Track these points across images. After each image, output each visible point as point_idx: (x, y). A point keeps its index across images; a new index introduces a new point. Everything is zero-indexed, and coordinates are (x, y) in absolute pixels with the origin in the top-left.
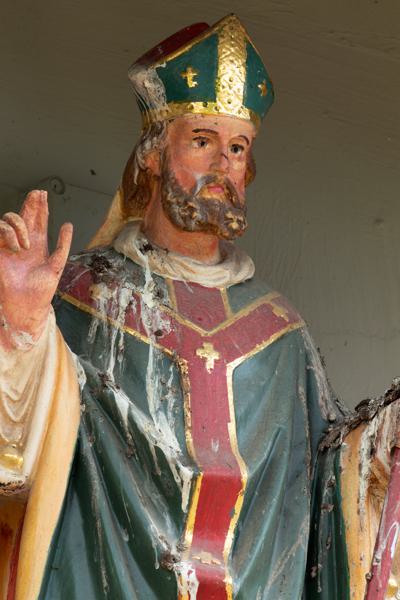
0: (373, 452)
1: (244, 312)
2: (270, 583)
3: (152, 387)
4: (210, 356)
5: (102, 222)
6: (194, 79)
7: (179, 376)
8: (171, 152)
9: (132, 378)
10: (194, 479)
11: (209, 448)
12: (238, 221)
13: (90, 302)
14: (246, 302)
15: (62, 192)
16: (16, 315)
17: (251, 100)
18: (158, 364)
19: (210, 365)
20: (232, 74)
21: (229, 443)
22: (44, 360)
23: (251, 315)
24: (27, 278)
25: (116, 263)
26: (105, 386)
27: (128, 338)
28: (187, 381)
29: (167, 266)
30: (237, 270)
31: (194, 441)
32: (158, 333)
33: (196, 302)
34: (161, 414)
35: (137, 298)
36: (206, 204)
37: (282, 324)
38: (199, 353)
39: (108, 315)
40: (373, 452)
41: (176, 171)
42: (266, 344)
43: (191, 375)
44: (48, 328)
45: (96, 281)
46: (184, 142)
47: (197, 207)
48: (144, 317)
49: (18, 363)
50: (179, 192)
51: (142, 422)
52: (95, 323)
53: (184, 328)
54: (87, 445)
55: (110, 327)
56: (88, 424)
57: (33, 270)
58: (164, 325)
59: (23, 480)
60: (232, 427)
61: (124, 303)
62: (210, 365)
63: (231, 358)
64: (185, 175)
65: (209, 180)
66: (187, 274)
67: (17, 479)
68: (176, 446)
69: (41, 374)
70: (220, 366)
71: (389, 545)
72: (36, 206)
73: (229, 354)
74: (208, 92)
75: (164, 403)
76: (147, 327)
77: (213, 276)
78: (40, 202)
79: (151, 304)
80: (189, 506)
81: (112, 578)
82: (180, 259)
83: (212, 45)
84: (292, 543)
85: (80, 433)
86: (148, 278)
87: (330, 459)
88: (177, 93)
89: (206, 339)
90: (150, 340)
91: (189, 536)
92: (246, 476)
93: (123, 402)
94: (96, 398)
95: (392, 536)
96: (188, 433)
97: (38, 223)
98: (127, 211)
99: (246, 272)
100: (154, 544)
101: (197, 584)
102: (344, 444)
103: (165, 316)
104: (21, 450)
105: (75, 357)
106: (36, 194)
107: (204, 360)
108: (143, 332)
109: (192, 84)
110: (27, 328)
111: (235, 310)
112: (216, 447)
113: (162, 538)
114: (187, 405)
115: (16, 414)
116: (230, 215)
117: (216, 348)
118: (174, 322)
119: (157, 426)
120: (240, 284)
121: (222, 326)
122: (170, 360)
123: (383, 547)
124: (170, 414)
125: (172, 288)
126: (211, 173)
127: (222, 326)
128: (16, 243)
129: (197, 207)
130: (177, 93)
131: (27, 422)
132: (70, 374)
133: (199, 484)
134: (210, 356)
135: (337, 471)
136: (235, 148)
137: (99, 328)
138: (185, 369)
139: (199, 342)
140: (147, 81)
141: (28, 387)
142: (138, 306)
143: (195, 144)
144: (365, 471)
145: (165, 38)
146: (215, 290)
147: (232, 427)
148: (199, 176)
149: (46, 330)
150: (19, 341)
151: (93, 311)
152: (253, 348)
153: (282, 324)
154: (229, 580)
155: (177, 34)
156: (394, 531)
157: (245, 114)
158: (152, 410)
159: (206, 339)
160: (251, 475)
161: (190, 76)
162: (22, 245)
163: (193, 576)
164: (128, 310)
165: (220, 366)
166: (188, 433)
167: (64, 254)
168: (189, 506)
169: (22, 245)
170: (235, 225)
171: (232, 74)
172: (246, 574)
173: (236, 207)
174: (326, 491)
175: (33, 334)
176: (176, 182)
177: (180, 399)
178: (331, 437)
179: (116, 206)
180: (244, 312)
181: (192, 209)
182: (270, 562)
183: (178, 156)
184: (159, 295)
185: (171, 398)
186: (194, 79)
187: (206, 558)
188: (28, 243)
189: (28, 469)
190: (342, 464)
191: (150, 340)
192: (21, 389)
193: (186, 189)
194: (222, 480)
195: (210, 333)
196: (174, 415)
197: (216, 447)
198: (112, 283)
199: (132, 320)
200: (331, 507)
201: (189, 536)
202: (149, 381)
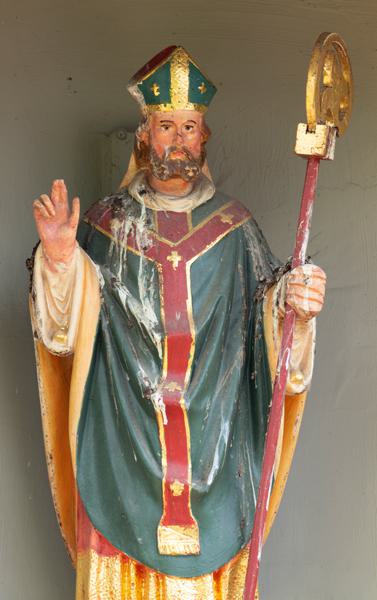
0: (278, 303)
1: (200, 226)
2: (217, 392)
3: (141, 283)
4: (175, 259)
5: (126, 171)
6: (158, 91)
7: (157, 274)
8: (152, 134)
9: (131, 279)
10: (162, 341)
11: (174, 317)
12: (193, 171)
13: (109, 230)
14: (201, 220)
15: (125, 138)
16: (54, 254)
17: (194, 96)
18: (145, 268)
19: (176, 264)
20: (180, 79)
21: (186, 313)
22: (75, 276)
23: (205, 227)
24: (57, 232)
25: (126, 202)
26: (113, 286)
27: (129, 253)
28: (161, 277)
29: (154, 203)
30: (199, 197)
31: (166, 315)
32: (145, 249)
33: (171, 224)
34: (147, 299)
35: (134, 226)
36: (172, 164)
37: (227, 226)
38: (168, 258)
39: (119, 239)
40: (278, 303)
41: (155, 145)
42: (213, 244)
43: (164, 273)
44: (78, 257)
45: (113, 216)
46: (157, 127)
47: (166, 167)
48: (138, 238)
49: (60, 280)
50: (156, 158)
51: (135, 309)
52: (112, 243)
53: (162, 244)
54: (105, 323)
55: (119, 246)
56: (105, 311)
57: (60, 227)
58: (149, 243)
59: (69, 350)
60: (189, 302)
61: (127, 231)
62: (176, 264)
63: (188, 259)
64: (160, 147)
65: (172, 149)
66: (166, 207)
67: (65, 349)
68: (154, 319)
69: (74, 285)
70: (182, 264)
71: (284, 363)
72: (58, 189)
73: (186, 254)
74: (166, 98)
75: (148, 292)
76: (139, 245)
77: (183, 205)
78: (60, 187)
79: (141, 230)
80: (163, 356)
81: (119, 405)
82: (161, 198)
83: (167, 68)
84: (231, 365)
85: (100, 316)
86: (143, 211)
87: (258, 306)
88: (151, 100)
89: (174, 249)
90: (140, 253)
91: (165, 373)
92: (194, 333)
93: (123, 294)
94: (109, 293)
95: (286, 357)
96: (162, 310)
97: (61, 197)
98: (138, 164)
99: (206, 196)
100: (140, 384)
101: (164, 406)
102: (308, 269)
103: (150, 237)
104: (66, 331)
105: (97, 267)
106: (56, 182)
107: (172, 262)
108: (137, 249)
109: (157, 94)
110: (61, 260)
111: (194, 226)
112: (178, 317)
113: (145, 379)
114: (162, 292)
115: (63, 308)
116: (187, 168)
117: (179, 254)
118: (155, 240)
119: (145, 308)
120: (203, 205)
121: (185, 238)
122: (151, 265)
123: (281, 364)
124: (152, 299)
125: (156, 216)
126: (174, 145)
127: (185, 238)
128: (47, 213)
129: (166, 167)
130: (151, 100)
131: (69, 312)
132: (92, 282)
133: (166, 343)
134: (175, 259)
135: (262, 313)
136: (188, 128)
137: (114, 247)
138: (160, 270)
139: (168, 251)
140: (134, 91)
141: (68, 293)
142: (135, 232)
143: (163, 129)
144: (276, 314)
145: (149, 60)
146: (184, 214)
147: (189, 302)
148: (167, 147)
149: (73, 261)
150: (60, 267)
151: (111, 236)
152: (204, 248)
153: (227, 226)
154: (182, 402)
155: (158, 56)
156: (287, 353)
157: (191, 106)
158: (141, 297)
159: (174, 249)
160: (198, 332)
161: (156, 89)
162: (50, 214)
163: (161, 401)
164: (129, 235)
165: (182, 264)
166: (162, 310)
167: (77, 215)
168: (163, 356)
169: (50, 214)
170: (191, 174)
171: (180, 79)
172: (194, 395)
173: (192, 162)
174: (257, 326)
175: (65, 263)
176: (155, 152)
177: (157, 288)
178: (260, 292)
179: (132, 162)
180: (200, 226)
181: (163, 169)
182: (218, 374)
183: (155, 137)
184: (148, 222)
185: (152, 290)
186: (158, 91)
187: (173, 387)
188: (54, 213)
189: (70, 344)
190: (264, 310)
191: (140, 253)
192: (64, 294)
193: (160, 156)
194: (179, 338)
195: (176, 244)
196: (154, 299)
197: (178, 317)
198: (122, 218)
199: (131, 242)
200: (260, 336)
201: (165, 373)
202: (139, 280)
